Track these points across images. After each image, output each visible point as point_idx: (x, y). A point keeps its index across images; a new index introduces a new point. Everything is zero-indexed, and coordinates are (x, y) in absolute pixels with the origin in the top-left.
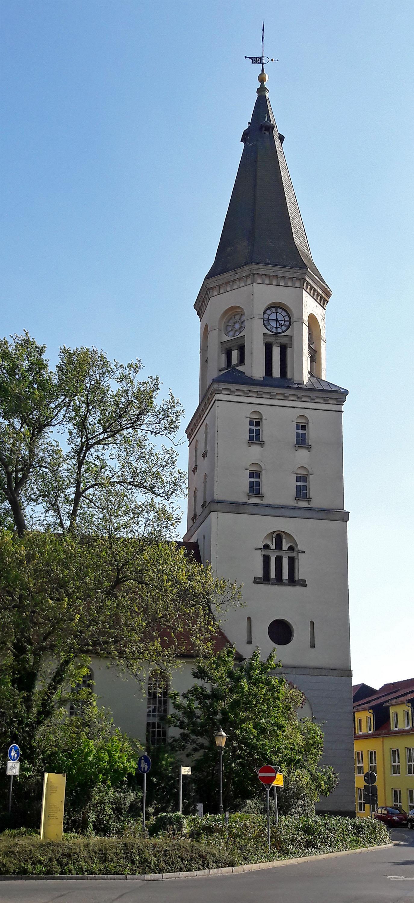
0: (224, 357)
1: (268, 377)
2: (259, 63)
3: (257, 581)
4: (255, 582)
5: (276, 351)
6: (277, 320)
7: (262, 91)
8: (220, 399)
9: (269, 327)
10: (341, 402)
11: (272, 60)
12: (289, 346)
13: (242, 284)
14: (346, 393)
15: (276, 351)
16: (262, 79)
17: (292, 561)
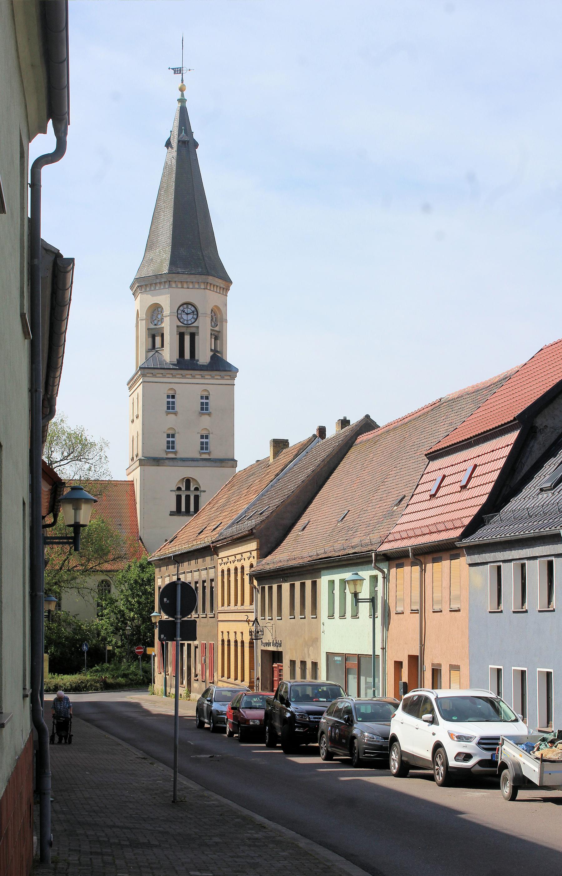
0: (150, 340)
1: (181, 359)
2: (179, 73)
3: (172, 514)
4: (170, 515)
5: (187, 339)
6: (187, 314)
7: (182, 101)
8: (146, 381)
9: (181, 320)
10: (233, 378)
11: (189, 70)
12: (196, 334)
13: (162, 287)
14: (237, 370)
15: (187, 339)
16: (182, 90)
17: (197, 498)
